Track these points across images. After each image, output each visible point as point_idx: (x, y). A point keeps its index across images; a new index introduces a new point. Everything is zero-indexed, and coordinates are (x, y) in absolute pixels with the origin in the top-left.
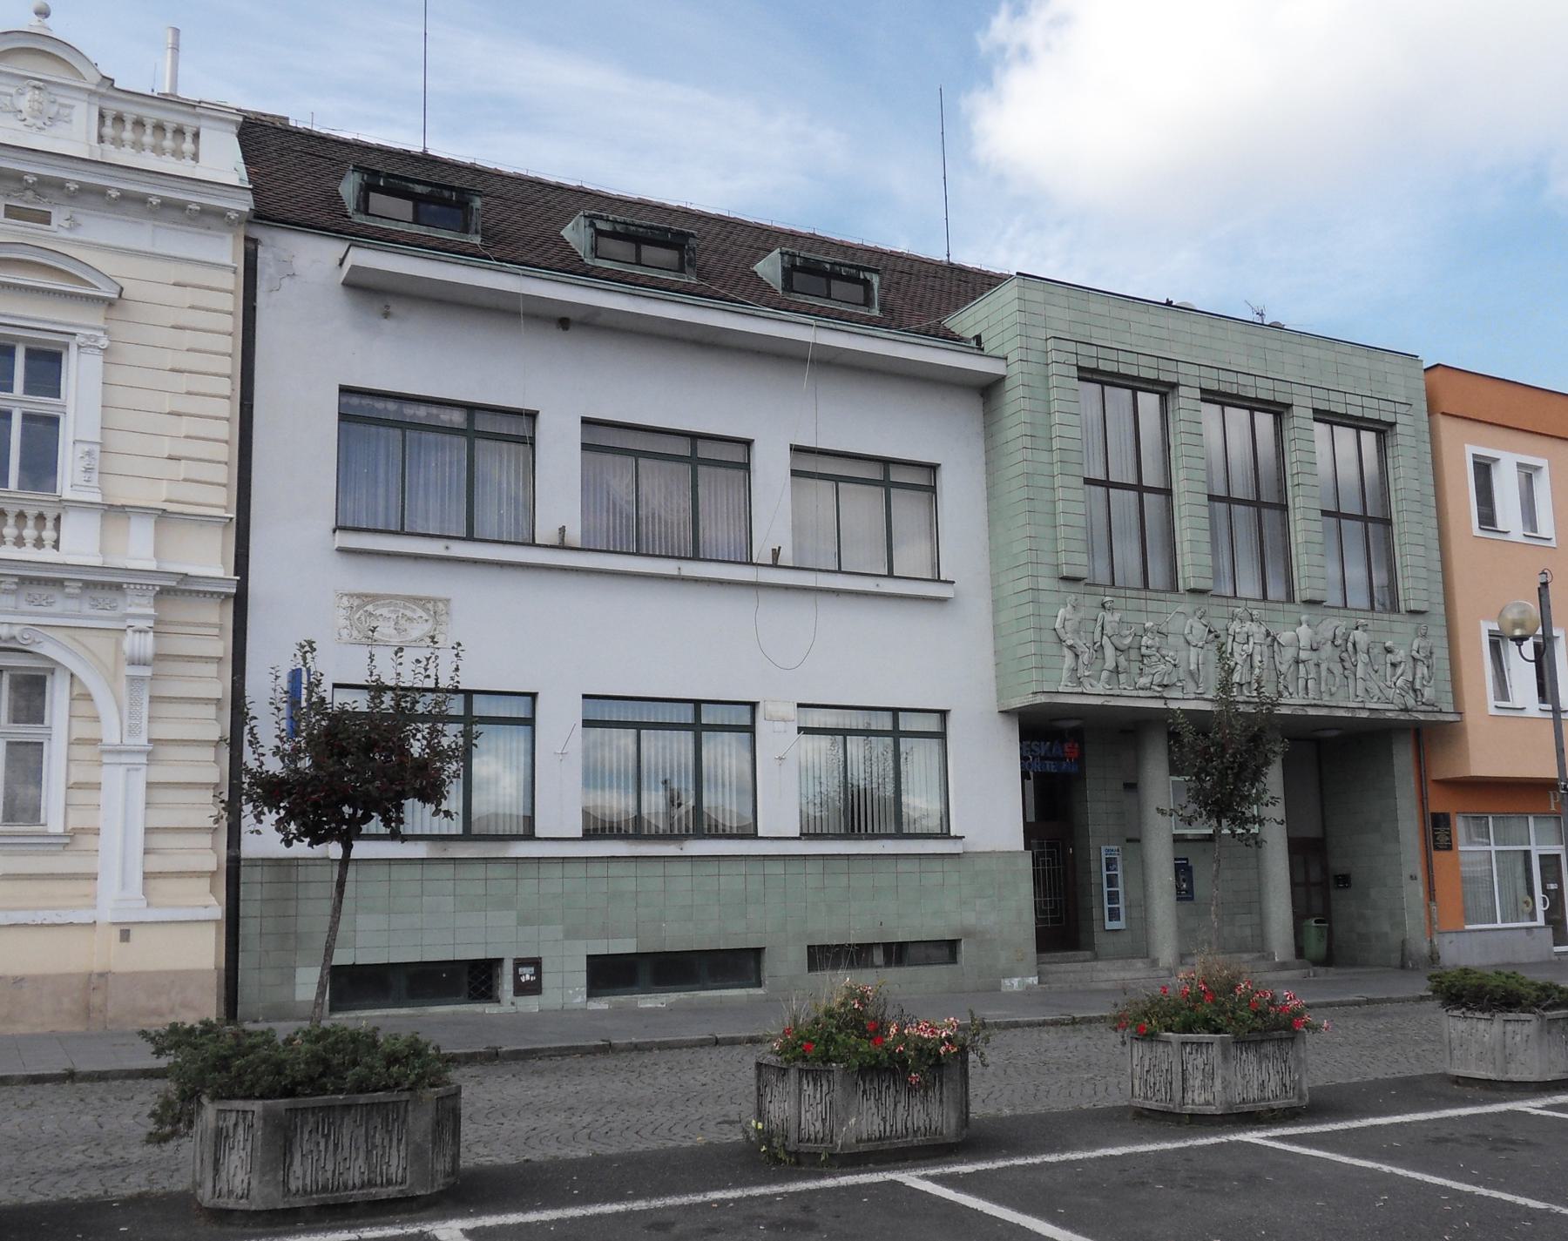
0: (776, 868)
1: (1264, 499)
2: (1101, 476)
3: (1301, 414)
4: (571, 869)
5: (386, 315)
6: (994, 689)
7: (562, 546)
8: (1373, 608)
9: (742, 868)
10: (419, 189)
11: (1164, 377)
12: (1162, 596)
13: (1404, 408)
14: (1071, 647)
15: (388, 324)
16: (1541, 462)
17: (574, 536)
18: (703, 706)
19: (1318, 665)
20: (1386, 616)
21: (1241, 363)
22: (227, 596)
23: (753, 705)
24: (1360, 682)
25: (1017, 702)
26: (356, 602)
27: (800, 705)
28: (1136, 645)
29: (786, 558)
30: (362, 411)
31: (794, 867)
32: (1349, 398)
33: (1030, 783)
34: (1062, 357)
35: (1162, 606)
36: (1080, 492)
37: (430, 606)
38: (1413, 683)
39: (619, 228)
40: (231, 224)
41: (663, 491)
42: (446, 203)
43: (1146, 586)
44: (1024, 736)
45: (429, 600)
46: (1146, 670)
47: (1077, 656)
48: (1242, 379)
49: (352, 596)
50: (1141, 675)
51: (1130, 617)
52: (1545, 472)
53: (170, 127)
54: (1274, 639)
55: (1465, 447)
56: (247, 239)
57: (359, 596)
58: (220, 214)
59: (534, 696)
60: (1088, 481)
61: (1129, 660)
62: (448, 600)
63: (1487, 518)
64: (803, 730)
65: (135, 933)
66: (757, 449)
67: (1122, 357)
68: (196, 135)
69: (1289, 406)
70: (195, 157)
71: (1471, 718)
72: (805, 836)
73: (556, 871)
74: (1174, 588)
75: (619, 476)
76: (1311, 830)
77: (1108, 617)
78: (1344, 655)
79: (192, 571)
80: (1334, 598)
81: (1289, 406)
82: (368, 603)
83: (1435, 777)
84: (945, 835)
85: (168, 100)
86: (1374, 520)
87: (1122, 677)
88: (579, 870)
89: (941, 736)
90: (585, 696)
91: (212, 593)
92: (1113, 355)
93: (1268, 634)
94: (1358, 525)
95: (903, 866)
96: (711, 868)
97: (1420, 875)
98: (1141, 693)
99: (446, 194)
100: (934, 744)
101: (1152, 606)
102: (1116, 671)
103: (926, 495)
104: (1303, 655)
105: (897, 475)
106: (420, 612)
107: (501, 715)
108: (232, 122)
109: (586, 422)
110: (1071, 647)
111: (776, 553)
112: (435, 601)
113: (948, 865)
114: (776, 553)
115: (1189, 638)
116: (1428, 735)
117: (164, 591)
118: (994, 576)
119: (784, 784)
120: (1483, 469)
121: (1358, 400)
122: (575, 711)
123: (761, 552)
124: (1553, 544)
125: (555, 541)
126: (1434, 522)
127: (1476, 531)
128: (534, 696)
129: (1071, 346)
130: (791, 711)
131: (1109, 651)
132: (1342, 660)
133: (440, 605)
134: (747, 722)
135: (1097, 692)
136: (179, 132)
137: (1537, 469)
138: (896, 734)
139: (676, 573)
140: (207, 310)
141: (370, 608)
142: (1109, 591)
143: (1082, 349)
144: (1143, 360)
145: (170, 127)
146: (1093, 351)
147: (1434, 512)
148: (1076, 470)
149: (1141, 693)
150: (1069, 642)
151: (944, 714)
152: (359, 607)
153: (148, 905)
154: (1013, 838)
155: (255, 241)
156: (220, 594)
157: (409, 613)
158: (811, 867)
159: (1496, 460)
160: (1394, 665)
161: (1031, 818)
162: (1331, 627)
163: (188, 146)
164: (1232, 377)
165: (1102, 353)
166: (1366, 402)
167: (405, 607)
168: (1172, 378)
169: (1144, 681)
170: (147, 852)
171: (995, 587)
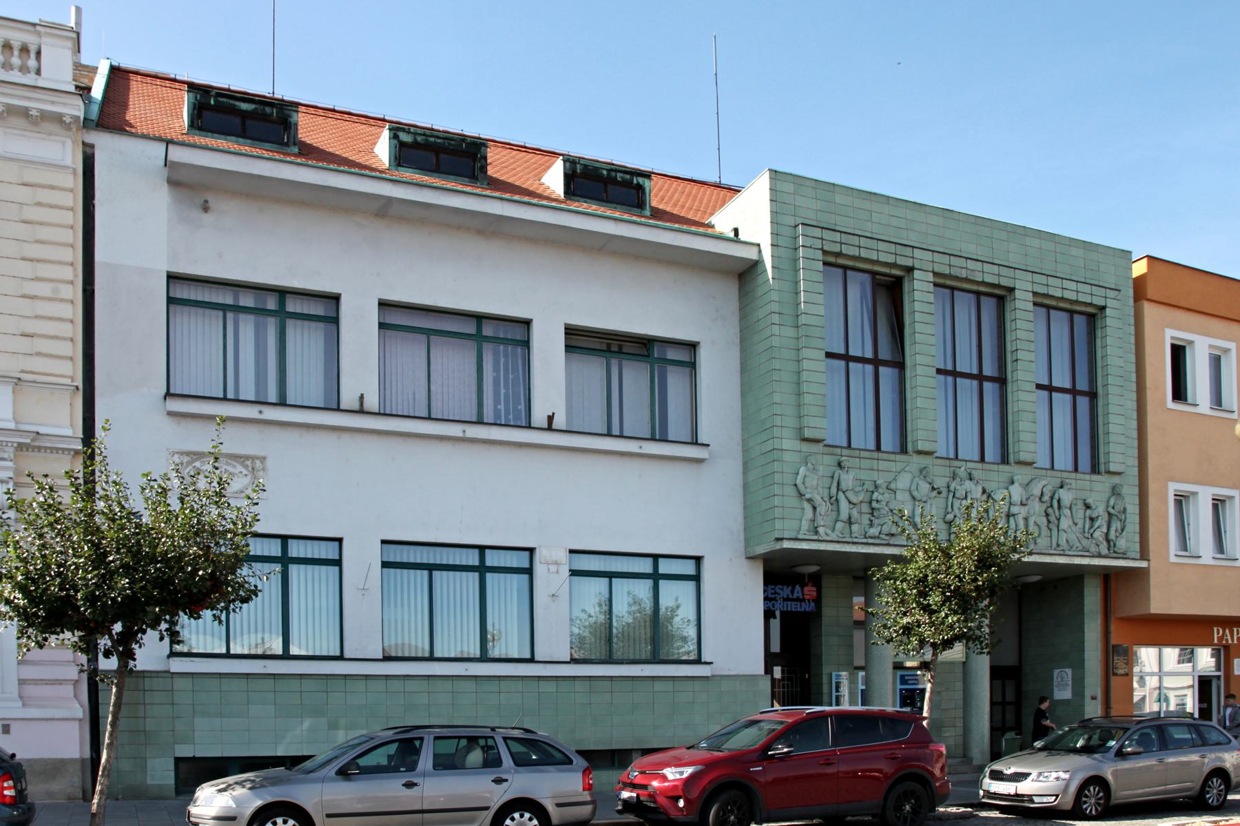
0: (551, 687)
1: (985, 373)
2: (1046, 383)
3: (1022, 302)
4: (372, 685)
5: (206, 208)
6: (742, 538)
7: (361, 411)
8: (1076, 470)
9: (519, 685)
10: (245, 106)
11: (901, 261)
12: (892, 457)
13: (1111, 294)
14: (809, 500)
15: (206, 218)
16: (1232, 346)
17: (372, 403)
18: (487, 551)
19: (1026, 519)
20: (1087, 477)
21: (970, 249)
22: (77, 452)
23: (531, 551)
24: (1062, 533)
25: (761, 549)
26: (186, 459)
27: (571, 551)
28: (867, 499)
29: (560, 422)
30: (185, 292)
31: (564, 686)
32: (1066, 284)
33: (776, 624)
34: (809, 242)
35: (892, 466)
36: (822, 364)
37: (249, 463)
38: (1107, 534)
39: (419, 139)
40: (68, 127)
41: (454, 365)
42: (266, 118)
43: (878, 448)
44: (767, 582)
45: (247, 457)
46: (876, 521)
47: (815, 508)
48: (971, 264)
49: (182, 453)
50: (871, 525)
51: (864, 475)
52: (1234, 353)
53: (16, 45)
54: (989, 496)
55: (1164, 330)
56: (84, 144)
57: (188, 454)
58: (58, 119)
59: (340, 540)
60: (829, 355)
61: (861, 513)
62: (264, 458)
63: (1179, 393)
64: (574, 573)
65: (14, 727)
66: (536, 329)
67: (863, 242)
68: (39, 53)
69: (1011, 290)
70: (38, 72)
71: (1155, 566)
72: (574, 661)
73: (361, 685)
74: (904, 450)
75: (409, 354)
76: (1010, 660)
77: (844, 476)
78: (1050, 510)
79: (42, 430)
80: (1043, 461)
81: (1011, 290)
82: (196, 460)
83: (1119, 615)
84: (698, 661)
85: (1017, 795)
86: (1082, 393)
87: (855, 527)
88: (381, 685)
89: (696, 578)
90: (383, 542)
91: (63, 450)
92: (855, 240)
93: (984, 491)
94: (1068, 397)
95: (659, 686)
96: (493, 686)
97: (1099, 695)
98: (870, 541)
99: (268, 110)
100: (691, 586)
101: (883, 465)
102: (850, 522)
103: (687, 370)
104: (1014, 510)
105: (292, 306)
106: (240, 468)
107: (631, 570)
108: (68, 38)
109: (383, 305)
110: (809, 500)
111: (551, 419)
112: (253, 458)
113: (697, 685)
114: (551, 419)
115: (915, 494)
116: (1119, 584)
117: (21, 447)
118: (744, 442)
119: (563, 614)
120: (1178, 353)
121: (1073, 286)
122: (375, 555)
123: (539, 418)
124: (1235, 416)
125: (356, 407)
126: (1134, 396)
127: (1170, 404)
128: (340, 540)
129: (817, 232)
130: (563, 556)
131: (844, 505)
132: (1047, 515)
133: (258, 463)
134: (527, 565)
135: (831, 540)
136: (24, 50)
137: (1227, 351)
138: (482, 570)
139: (461, 435)
140: (52, 207)
141: (197, 464)
142: (845, 452)
143: (827, 235)
144: (882, 246)
145: (16, 45)
146: (837, 237)
147: (1134, 387)
148: (820, 344)
149: (870, 541)
150: (808, 496)
151: (698, 560)
152: (189, 463)
153: (24, 705)
154: (754, 663)
155: (92, 146)
156: (69, 450)
157: (231, 469)
158: (579, 686)
159: (1191, 343)
160: (1092, 520)
161: (776, 647)
162: (1040, 486)
163: (32, 63)
164: (962, 262)
165: (845, 238)
166: (1081, 287)
167: (227, 464)
168: (909, 263)
169: (874, 531)
170: (20, 663)
171: (745, 450)
